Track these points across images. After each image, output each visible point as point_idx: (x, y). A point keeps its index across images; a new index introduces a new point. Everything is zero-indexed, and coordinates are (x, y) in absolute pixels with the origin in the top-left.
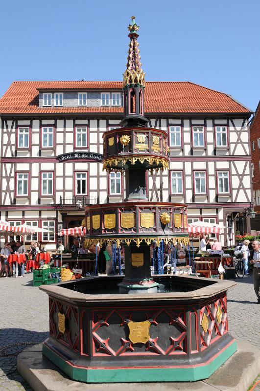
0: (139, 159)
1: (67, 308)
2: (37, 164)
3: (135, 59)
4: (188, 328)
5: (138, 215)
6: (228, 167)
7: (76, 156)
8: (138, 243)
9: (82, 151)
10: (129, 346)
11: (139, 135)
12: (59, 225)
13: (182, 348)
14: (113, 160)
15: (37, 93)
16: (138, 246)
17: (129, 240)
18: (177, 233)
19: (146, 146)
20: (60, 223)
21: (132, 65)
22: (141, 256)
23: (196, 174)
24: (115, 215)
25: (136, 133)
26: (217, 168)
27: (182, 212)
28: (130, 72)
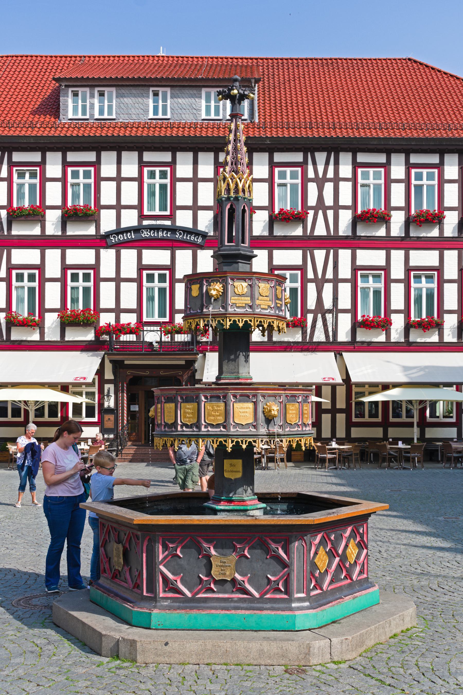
0: (237, 319)
1: (125, 534)
2: (57, 252)
3: (237, 155)
4: (292, 563)
5: (230, 406)
6: (299, 262)
7: (145, 234)
8: (230, 446)
9: (159, 222)
10: (210, 585)
11: (237, 284)
12: (107, 386)
13: (283, 590)
14: (197, 320)
15: (54, 85)
16: (229, 450)
17: (217, 441)
18: (305, 431)
19: (248, 300)
20: (109, 382)
21: (232, 164)
22: (239, 463)
23: (415, 277)
24: (196, 404)
25: (233, 279)
26: (144, 263)
27: (300, 400)
28: (227, 175)
